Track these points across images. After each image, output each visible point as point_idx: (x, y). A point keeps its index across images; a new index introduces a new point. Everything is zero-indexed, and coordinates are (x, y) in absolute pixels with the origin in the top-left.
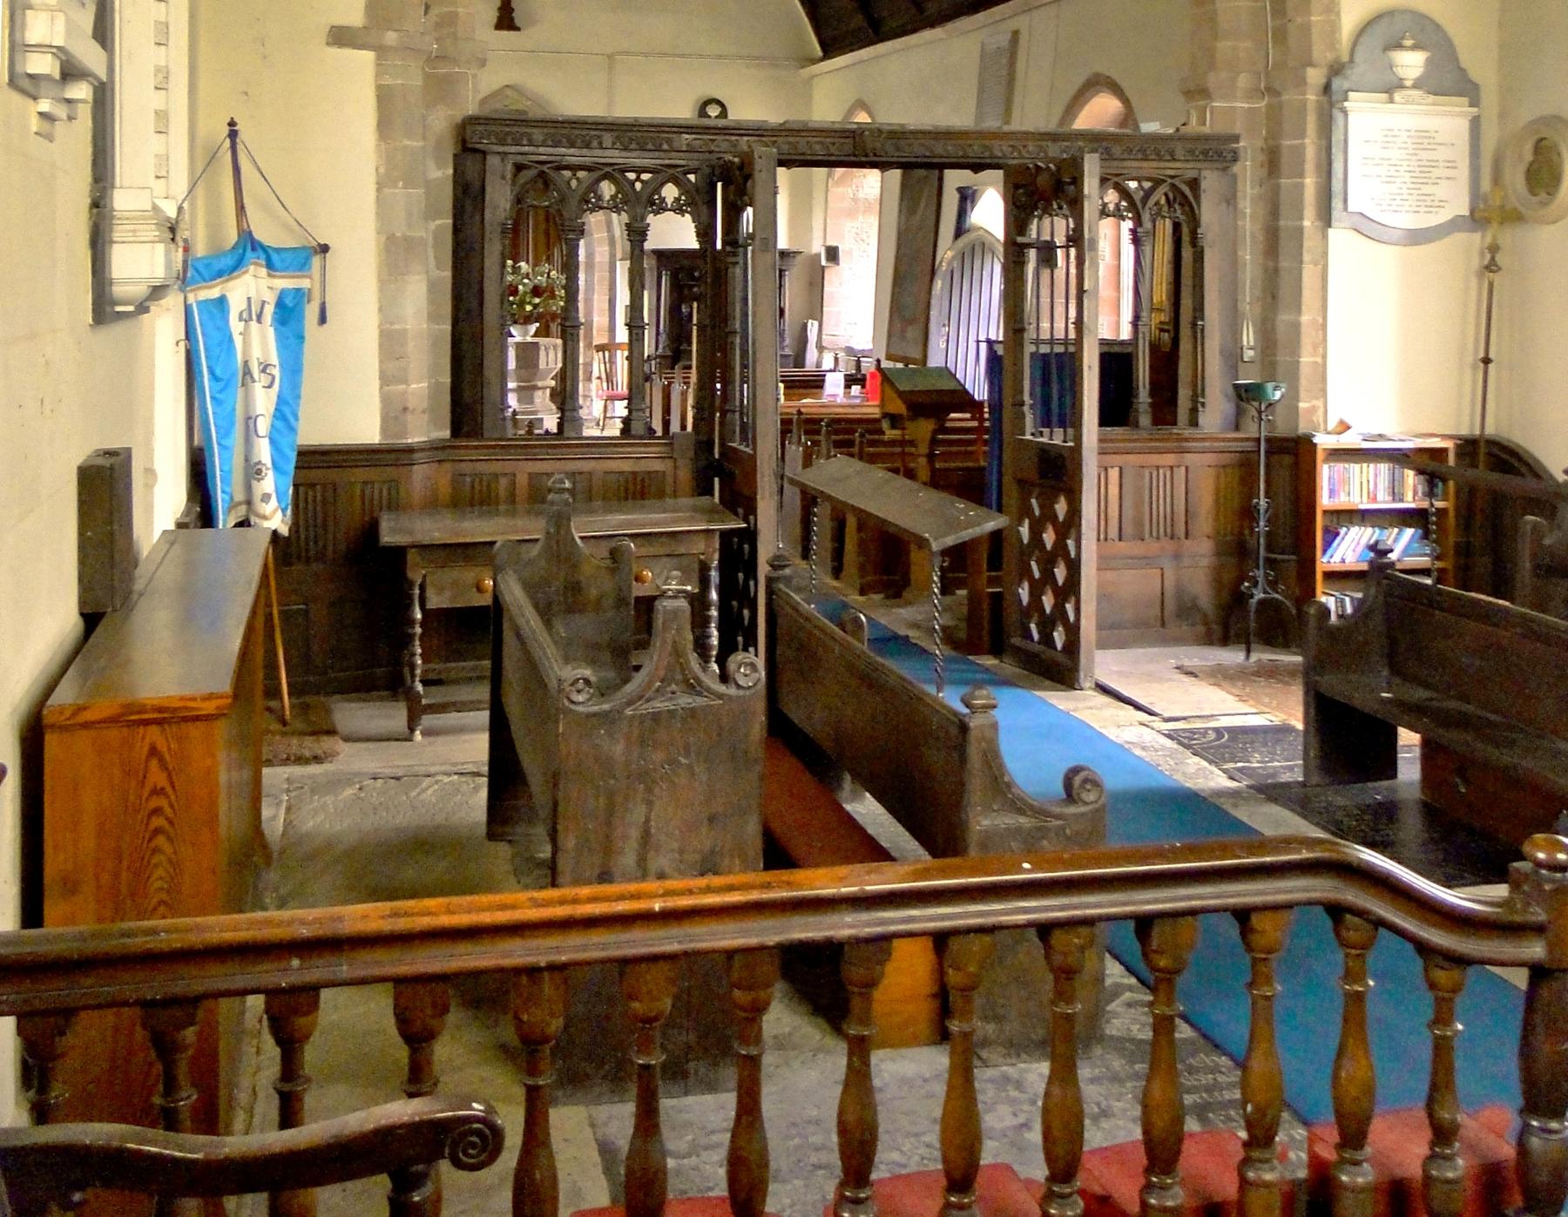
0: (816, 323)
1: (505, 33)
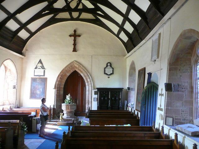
0: (126, 101)
1: (75, 53)
